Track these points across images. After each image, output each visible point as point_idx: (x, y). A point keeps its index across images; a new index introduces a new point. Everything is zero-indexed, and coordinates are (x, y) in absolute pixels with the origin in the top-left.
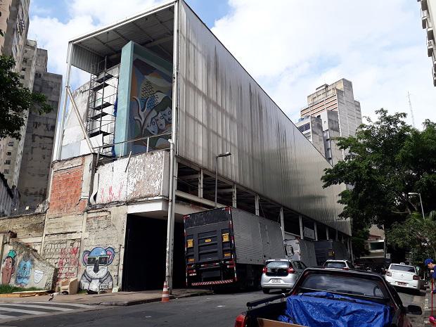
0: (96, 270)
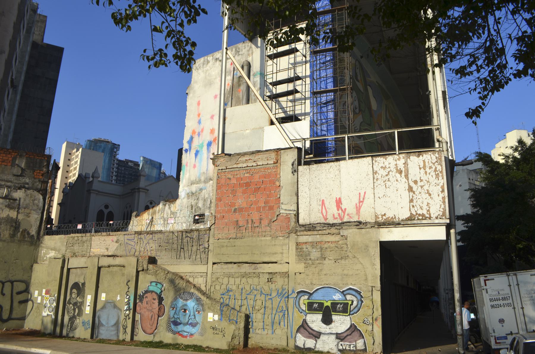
0: (327, 320)
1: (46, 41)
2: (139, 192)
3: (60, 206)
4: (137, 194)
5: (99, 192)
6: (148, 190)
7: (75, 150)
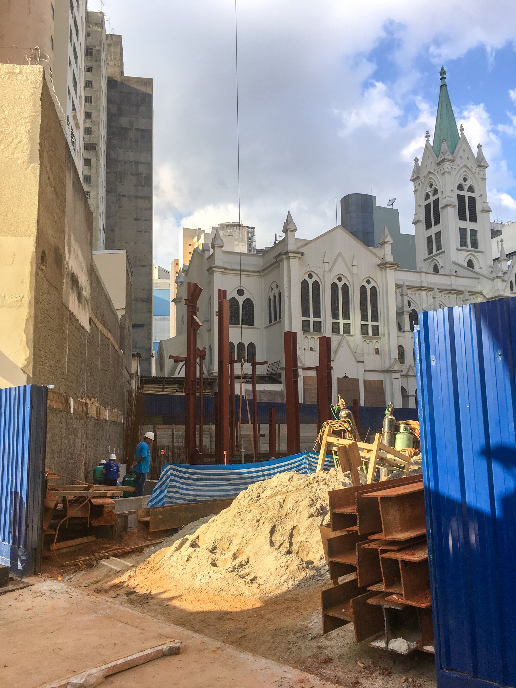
2: (288, 258)
4: (285, 262)
5: (226, 269)
6: (302, 254)
7: (196, 238)
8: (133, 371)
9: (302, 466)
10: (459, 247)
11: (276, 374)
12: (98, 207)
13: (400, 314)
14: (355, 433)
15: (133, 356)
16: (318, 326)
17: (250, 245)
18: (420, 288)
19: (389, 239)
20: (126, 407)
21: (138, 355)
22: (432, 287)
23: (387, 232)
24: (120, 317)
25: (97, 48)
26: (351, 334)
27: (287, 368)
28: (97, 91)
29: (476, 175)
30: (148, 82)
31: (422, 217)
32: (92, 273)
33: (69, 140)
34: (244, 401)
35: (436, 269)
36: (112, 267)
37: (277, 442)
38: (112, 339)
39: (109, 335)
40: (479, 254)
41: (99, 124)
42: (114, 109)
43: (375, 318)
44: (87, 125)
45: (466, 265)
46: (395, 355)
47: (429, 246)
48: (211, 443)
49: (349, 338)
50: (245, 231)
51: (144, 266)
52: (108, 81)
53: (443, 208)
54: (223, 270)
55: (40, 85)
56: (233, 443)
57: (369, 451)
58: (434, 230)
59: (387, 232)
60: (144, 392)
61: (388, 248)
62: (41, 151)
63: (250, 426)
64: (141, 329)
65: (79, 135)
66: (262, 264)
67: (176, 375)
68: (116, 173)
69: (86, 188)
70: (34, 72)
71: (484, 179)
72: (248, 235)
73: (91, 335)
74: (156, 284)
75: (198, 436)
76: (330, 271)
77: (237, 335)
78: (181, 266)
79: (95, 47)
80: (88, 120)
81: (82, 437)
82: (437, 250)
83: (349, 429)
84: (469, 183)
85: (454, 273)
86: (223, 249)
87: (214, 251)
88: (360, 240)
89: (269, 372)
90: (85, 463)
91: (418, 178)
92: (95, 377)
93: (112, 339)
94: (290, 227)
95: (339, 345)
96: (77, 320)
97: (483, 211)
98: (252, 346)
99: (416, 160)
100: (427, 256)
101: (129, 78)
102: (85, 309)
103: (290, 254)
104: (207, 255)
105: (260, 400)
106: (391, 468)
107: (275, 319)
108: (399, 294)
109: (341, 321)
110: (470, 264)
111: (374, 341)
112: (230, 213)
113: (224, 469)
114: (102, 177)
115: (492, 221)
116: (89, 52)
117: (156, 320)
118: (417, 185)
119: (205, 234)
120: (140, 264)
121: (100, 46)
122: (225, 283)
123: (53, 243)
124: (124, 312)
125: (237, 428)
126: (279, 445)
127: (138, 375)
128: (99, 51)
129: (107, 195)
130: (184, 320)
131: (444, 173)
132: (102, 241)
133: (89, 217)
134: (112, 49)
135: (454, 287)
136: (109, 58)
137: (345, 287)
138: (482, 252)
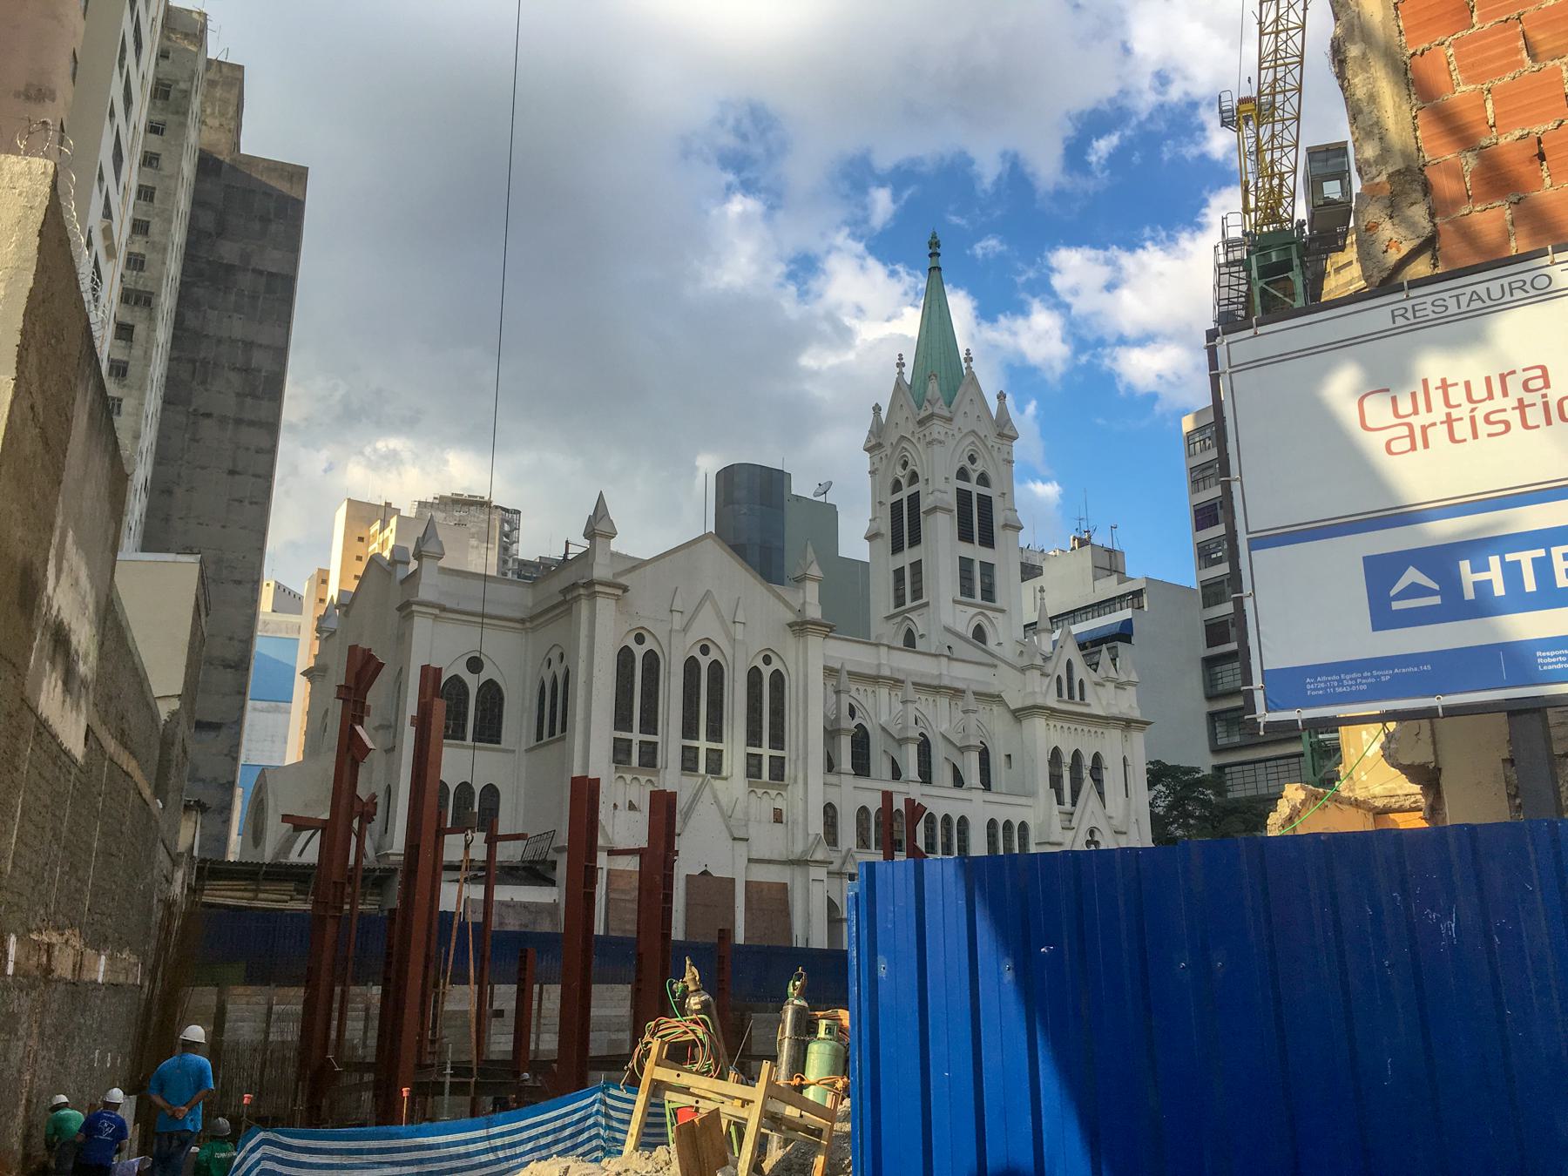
1: (594, 987)
2: (593, 596)
3: (311, 680)
4: (584, 606)
5: (443, 609)
6: (625, 589)
7: (377, 526)
8: (182, 846)
9: (591, 1121)
10: (959, 597)
11: (544, 862)
12: (137, 437)
13: (831, 734)
14: (717, 1049)
15: (187, 808)
16: (649, 756)
17: (505, 549)
18: (875, 680)
19: (815, 570)
20: (153, 943)
21: (201, 807)
22: (901, 677)
23: (811, 555)
24: (164, 716)
25: (182, 86)
26: (724, 774)
27: (572, 849)
28: (170, 177)
29: (995, 453)
30: (299, 175)
31: (886, 527)
32: (110, 618)
33: (86, 284)
34: (463, 926)
35: (910, 641)
36: (160, 597)
37: (533, 1029)
38: (138, 775)
39: (131, 765)
40: (997, 615)
41: (165, 249)
42: (208, 221)
43: (778, 741)
44: (136, 249)
45: (970, 635)
46: (817, 826)
47: (896, 590)
48: (365, 1032)
49: (718, 784)
50: (496, 517)
51: (239, 582)
52: (200, 158)
53: (928, 512)
54: (437, 612)
55: (42, 201)
56: (422, 1035)
57: (745, 1102)
58: (907, 557)
59: (811, 555)
60: (205, 899)
61: (812, 591)
62: (23, 349)
63: (472, 989)
64: (213, 734)
65: (113, 273)
66: (530, 604)
67: (293, 858)
68: (193, 361)
69: (112, 389)
70: (30, 173)
71: (1010, 462)
72: (502, 527)
73: (85, 770)
74: (266, 623)
75: (336, 1014)
76: (685, 630)
77: (459, 764)
78: (333, 591)
79: (177, 82)
80: (138, 238)
81: (29, 1036)
82: (914, 600)
83: (706, 1040)
84: (979, 467)
85: (947, 652)
86: (441, 563)
87: (420, 565)
88: (754, 568)
89: (529, 856)
90: (29, 1101)
91: (879, 445)
92: (80, 873)
93: (138, 775)
94: (601, 527)
95: (695, 798)
96: (54, 737)
97: (1006, 526)
98: (491, 792)
99: (877, 409)
100: (893, 611)
101: (251, 160)
102: (78, 705)
103: (598, 588)
104: (401, 573)
105: (501, 924)
106: (792, 1134)
107: (552, 733)
108: (830, 689)
109: (703, 744)
110: (979, 634)
111: (773, 793)
112: (462, 472)
113: (399, 1137)
114: (158, 369)
115: (1023, 544)
116: (161, 91)
117: (255, 709)
118: (877, 459)
119: (400, 517)
120: (230, 581)
121: (190, 81)
122: (436, 645)
123: (20, 558)
124: (175, 705)
125: (437, 994)
126: (538, 1038)
127: (192, 857)
128: (186, 94)
129: (163, 410)
130: (329, 720)
131: (930, 443)
132: (137, 514)
133: (119, 479)
134: (218, 92)
135: (946, 682)
136: (209, 111)
137: (716, 670)
138: (1002, 611)
